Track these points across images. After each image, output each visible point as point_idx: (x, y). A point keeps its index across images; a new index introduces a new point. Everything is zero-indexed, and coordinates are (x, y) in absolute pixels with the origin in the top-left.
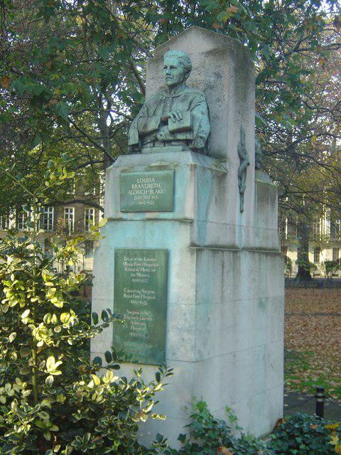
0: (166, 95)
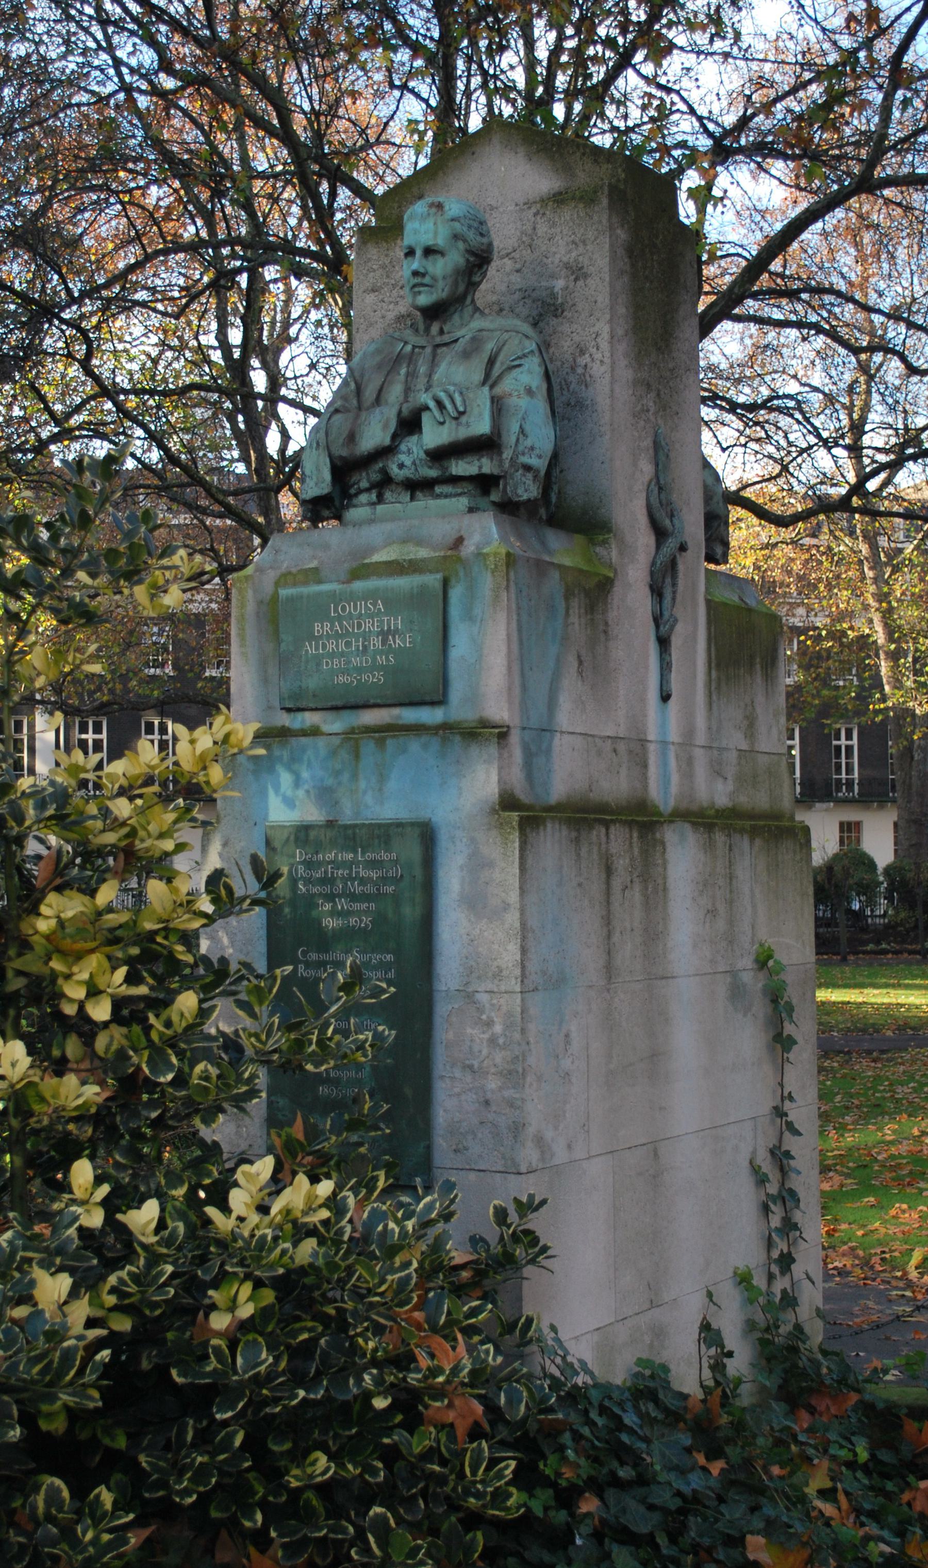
0: (414, 339)
